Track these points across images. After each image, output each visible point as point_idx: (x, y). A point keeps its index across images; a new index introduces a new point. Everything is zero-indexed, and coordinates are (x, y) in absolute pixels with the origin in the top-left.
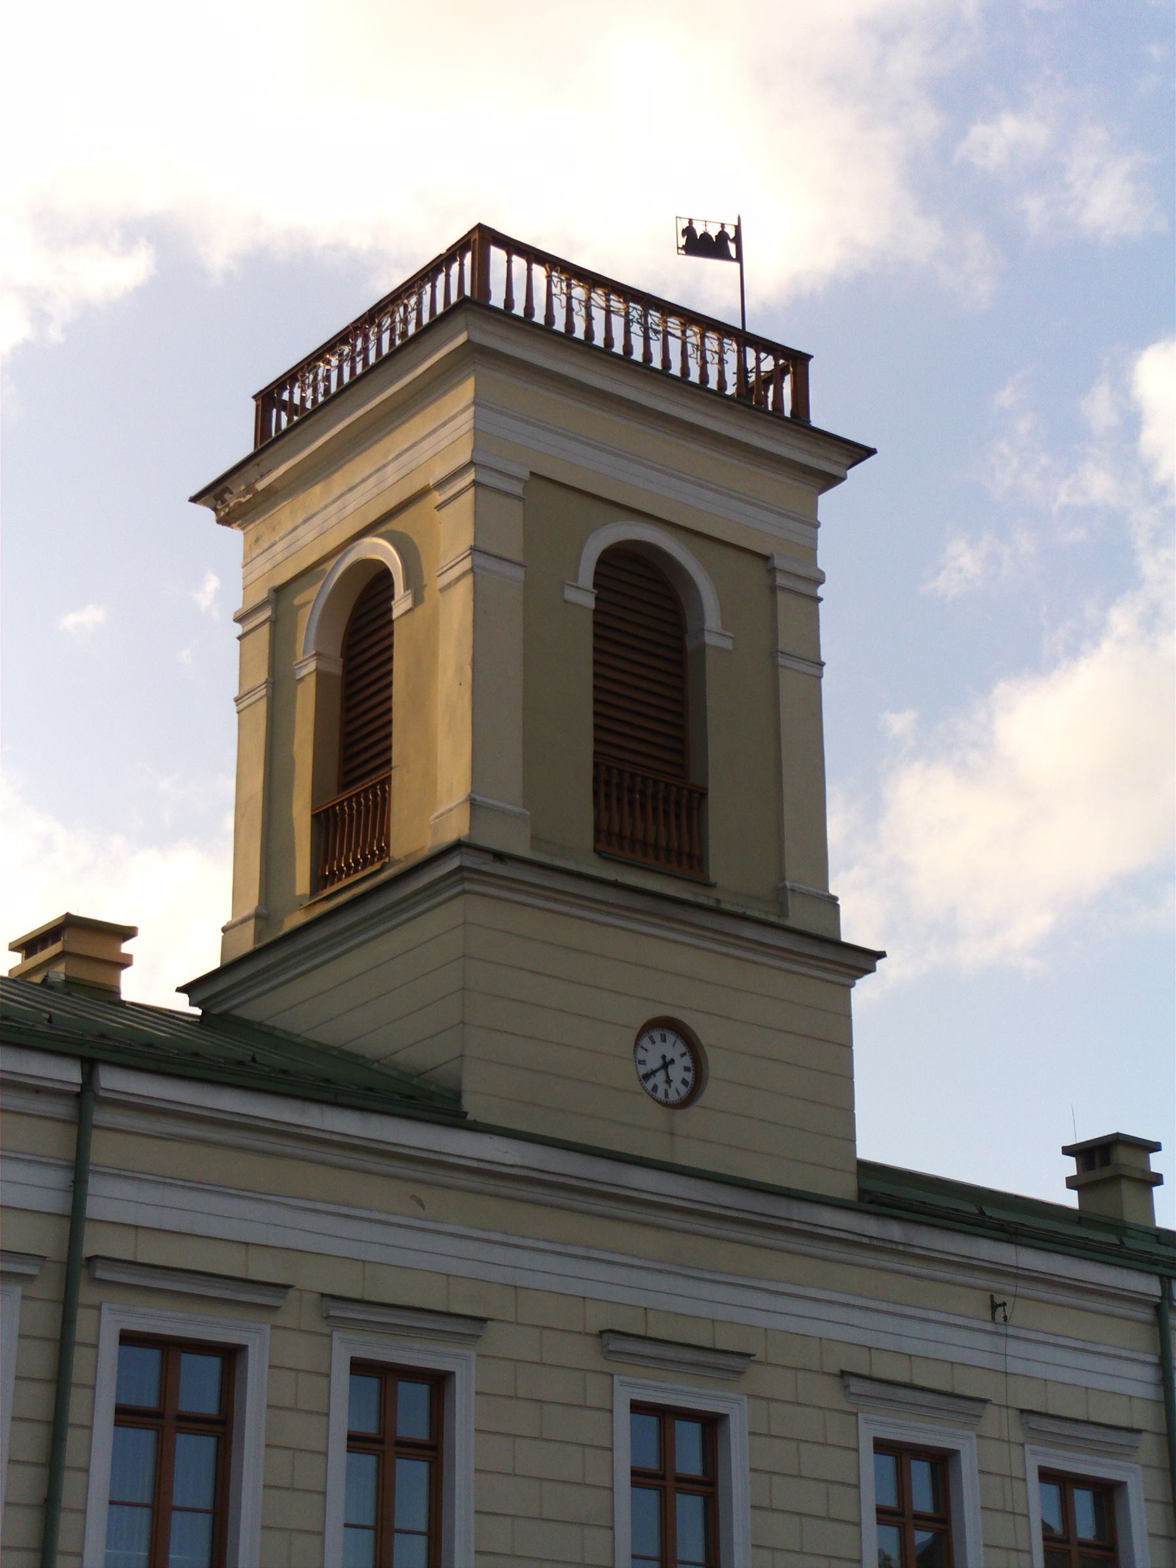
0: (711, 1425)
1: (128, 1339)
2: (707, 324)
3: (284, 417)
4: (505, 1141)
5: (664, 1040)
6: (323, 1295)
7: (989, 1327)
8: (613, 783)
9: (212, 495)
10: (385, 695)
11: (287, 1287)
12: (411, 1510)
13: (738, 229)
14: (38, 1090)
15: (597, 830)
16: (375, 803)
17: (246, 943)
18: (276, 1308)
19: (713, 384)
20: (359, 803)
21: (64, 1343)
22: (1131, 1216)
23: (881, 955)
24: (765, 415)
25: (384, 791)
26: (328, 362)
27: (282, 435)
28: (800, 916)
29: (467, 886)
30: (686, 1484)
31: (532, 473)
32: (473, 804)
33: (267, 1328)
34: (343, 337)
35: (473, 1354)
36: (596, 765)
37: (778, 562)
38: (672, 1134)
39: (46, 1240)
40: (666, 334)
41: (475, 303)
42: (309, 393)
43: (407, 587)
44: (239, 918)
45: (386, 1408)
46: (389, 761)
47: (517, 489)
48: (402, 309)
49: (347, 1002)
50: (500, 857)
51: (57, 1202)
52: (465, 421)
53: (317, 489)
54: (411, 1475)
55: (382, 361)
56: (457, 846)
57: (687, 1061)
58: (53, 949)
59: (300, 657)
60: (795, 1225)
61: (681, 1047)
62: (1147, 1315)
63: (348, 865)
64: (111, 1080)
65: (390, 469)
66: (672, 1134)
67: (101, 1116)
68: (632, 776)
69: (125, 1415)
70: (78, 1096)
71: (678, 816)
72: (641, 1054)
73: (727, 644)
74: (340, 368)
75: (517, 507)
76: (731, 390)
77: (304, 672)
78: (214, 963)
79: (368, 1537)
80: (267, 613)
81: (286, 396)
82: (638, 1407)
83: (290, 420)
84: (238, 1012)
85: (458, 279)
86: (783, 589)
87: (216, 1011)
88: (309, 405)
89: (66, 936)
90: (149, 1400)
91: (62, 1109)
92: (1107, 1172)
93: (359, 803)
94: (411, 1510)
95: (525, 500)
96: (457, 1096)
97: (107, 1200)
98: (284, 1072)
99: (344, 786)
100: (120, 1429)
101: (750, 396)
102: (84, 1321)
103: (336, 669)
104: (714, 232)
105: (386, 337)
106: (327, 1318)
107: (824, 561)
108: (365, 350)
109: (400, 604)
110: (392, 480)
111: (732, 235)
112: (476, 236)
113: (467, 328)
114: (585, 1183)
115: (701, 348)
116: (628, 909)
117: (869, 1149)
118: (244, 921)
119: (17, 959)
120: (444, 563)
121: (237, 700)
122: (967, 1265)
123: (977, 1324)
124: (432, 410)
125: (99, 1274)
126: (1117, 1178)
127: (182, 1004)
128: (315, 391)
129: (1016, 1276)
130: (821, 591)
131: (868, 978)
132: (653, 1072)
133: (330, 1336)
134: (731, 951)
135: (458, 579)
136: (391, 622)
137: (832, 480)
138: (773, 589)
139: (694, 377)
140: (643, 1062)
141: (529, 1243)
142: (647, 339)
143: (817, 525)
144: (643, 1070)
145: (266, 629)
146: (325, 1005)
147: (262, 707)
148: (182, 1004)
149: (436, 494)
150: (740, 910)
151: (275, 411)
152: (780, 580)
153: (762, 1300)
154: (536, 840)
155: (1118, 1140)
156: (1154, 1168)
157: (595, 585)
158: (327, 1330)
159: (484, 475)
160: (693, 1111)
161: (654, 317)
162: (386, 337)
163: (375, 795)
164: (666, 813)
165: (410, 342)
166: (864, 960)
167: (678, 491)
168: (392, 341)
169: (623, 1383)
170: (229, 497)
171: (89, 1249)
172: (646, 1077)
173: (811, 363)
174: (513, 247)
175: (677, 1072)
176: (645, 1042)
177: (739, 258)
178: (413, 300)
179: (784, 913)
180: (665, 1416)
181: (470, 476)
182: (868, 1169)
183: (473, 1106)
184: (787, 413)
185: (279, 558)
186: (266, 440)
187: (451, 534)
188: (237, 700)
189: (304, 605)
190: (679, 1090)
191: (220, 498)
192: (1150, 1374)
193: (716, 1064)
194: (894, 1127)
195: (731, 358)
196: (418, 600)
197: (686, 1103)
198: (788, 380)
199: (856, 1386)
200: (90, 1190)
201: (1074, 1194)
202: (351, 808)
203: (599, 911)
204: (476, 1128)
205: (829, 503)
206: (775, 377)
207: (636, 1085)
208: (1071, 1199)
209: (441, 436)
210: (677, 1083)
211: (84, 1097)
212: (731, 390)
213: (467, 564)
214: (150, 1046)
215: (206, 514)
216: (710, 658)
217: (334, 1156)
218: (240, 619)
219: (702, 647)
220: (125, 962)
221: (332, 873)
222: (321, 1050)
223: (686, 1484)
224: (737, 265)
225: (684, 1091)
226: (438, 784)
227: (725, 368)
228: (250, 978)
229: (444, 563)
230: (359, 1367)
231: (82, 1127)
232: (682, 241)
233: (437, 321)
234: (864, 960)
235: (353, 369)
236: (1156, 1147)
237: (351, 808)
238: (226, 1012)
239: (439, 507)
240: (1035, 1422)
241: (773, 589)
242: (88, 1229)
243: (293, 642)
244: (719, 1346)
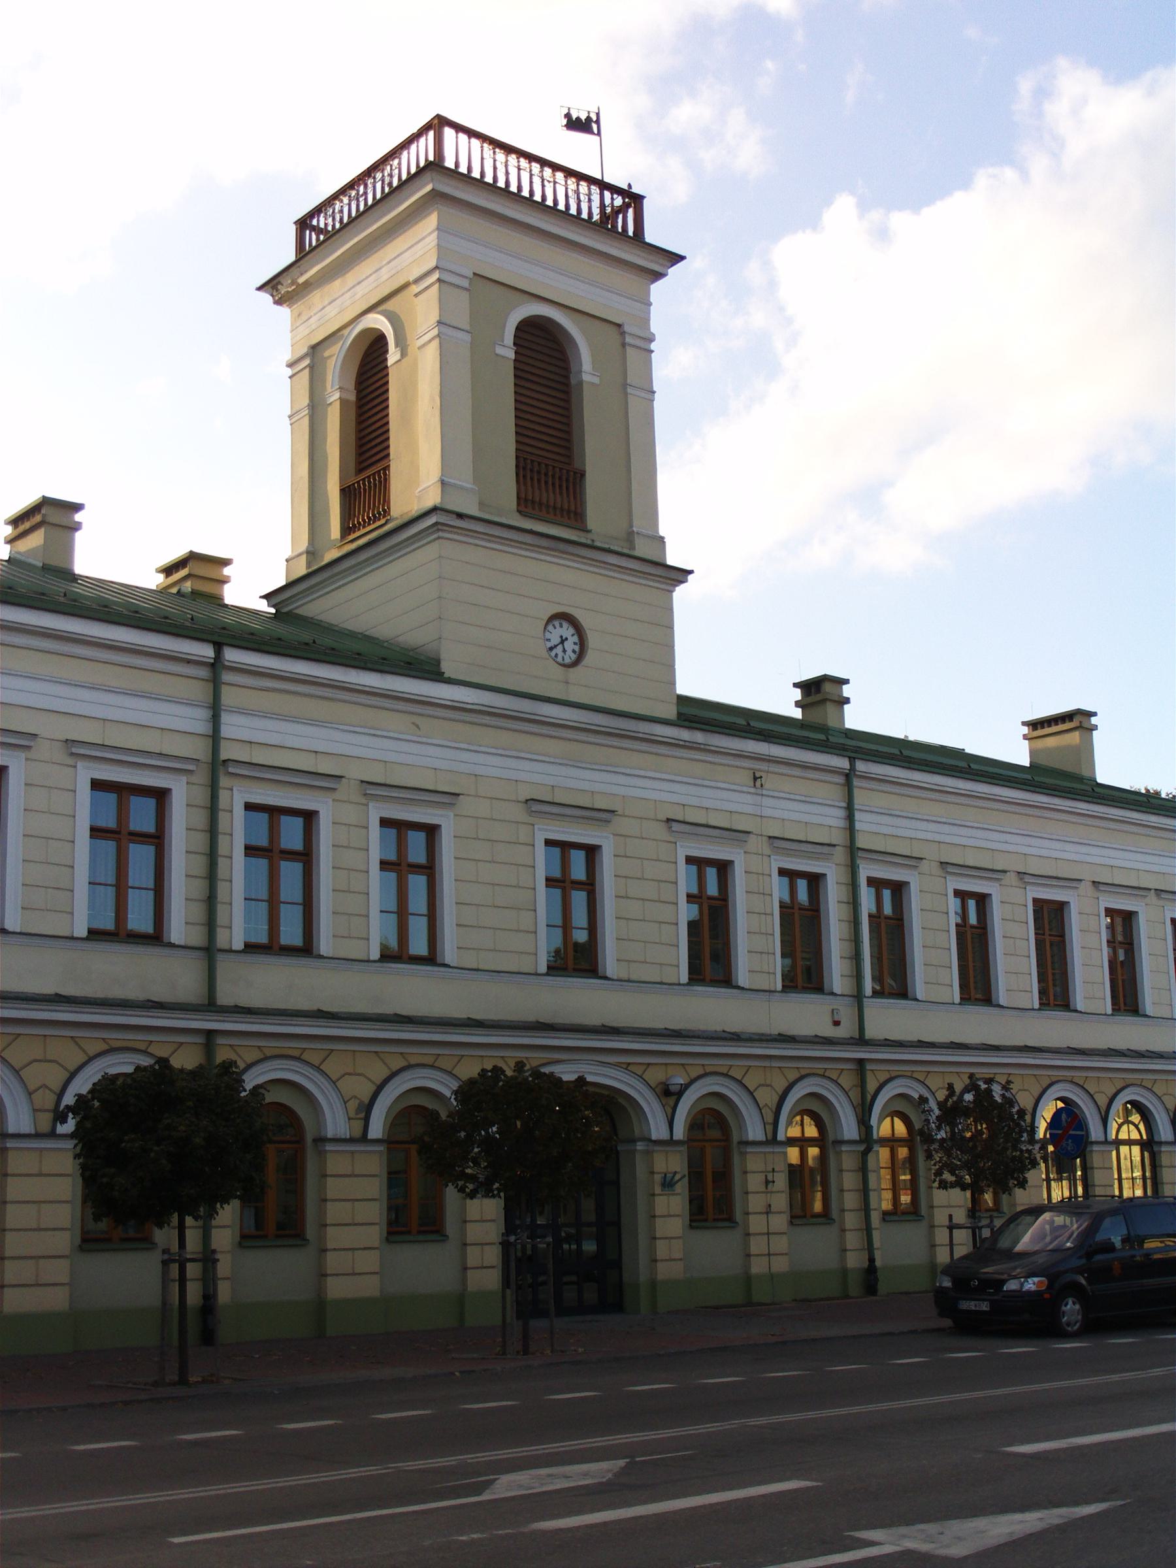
0: (592, 852)
1: (249, 807)
2: (580, 177)
3: (314, 236)
4: (503, 696)
5: (561, 626)
6: (362, 781)
7: (752, 790)
8: (526, 468)
9: (271, 285)
10: (384, 413)
11: (342, 777)
12: (418, 901)
13: (598, 114)
14: (189, 662)
15: (518, 498)
16: (380, 482)
17: (301, 570)
18: (28, 748)
19: (585, 215)
20: (369, 482)
21: (213, 809)
22: (832, 723)
23: (691, 572)
24: (617, 231)
25: (385, 474)
26: (342, 201)
27: (313, 249)
28: (642, 549)
29: (441, 534)
30: (577, 885)
31: (475, 274)
32: (443, 483)
33: (330, 801)
34: (351, 185)
35: (452, 814)
36: (517, 457)
37: (626, 328)
38: (567, 683)
39: (199, 750)
40: (555, 183)
41: (435, 166)
42: (330, 221)
43: (397, 346)
44: (296, 553)
45: (274, 831)
46: (388, 455)
47: (465, 283)
48: (389, 168)
49: (372, 603)
50: (460, 516)
51: (203, 727)
52: (432, 241)
53: (337, 283)
54: (141, 857)
55: (376, 203)
56: (434, 510)
57: (576, 639)
58: (183, 573)
59: (329, 389)
60: (641, 735)
61: (572, 630)
62: (841, 780)
63: (364, 520)
64: (232, 655)
65: (384, 270)
66: (567, 683)
67: (227, 677)
68: (539, 464)
69: (251, 850)
70: (213, 665)
71: (567, 488)
72: (548, 635)
73: (596, 380)
74: (349, 205)
75: (466, 295)
76: (596, 217)
77: (332, 399)
78: (284, 583)
79: (393, 918)
80: (307, 362)
81: (315, 222)
82: (549, 843)
83: (318, 239)
84: (296, 611)
85: (423, 150)
86: (630, 345)
87: (285, 610)
88: (330, 228)
89: (190, 564)
90: (263, 842)
91: (204, 673)
92: (818, 697)
93: (369, 482)
94: (418, 901)
95: (472, 289)
96: (438, 662)
97: (232, 725)
98: (333, 649)
99: (360, 471)
100: (253, 860)
101: (606, 223)
102: (223, 795)
103: (352, 397)
104: (583, 117)
105: (379, 186)
106: (72, 754)
107: (654, 328)
108: (365, 193)
109: (393, 356)
110: (385, 277)
111: (594, 118)
112: (436, 121)
113: (432, 180)
114: (516, 712)
115: (577, 192)
116: (539, 547)
117: (684, 687)
118: (300, 555)
119: (161, 578)
120: (420, 331)
121: (290, 417)
122: (740, 755)
123: (745, 789)
124: (410, 233)
125: (231, 770)
126: (824, 701)
127: (263, 606)
128: (334, 219)
129: (769, 761)
130: (653, 346)
131: (683, 586)
132: (556, 646)
133: (367, 805)
134: (602, 571)
135: (430, 341)
136: (387, 367)
137: (658, 276)
138: (624, 345)
139: (573, 211)
140: (549, 640)
141: (483, 749)
142: (543, 186)
143: (650, 304)
144: (549, 645)
145: (307, 371)
146: (352, 606)
147: (306, 420)
148: (263, 606)
149: (414, 287)
150: (606, 546)
151: (308, 232)
152: (628, 339)
153: (621, 779)
154: (482, 505)
155: (825, 679)
156: (845, 695)
157: (515, 344)
158: (364, 801)
159: (445, 275)
160: (579, 668)
161: (548, 172)
162: (379, 186)
163: (380, 477)
164: (560, 486)
165: (393, 191)
166: (681, 575)
167: (564, 284)
168: (383, 188)
169: (540, 829)
170: (279, 287)
171: (224, 755)
172: (551, 649)
173: (645, 201)
174: (459, 128)
175: (569, 645)
176: (550, 627)
177: (599, 134)
178: (396, 162)
179: (633, 548)
180: (565, 847)
181: (436, 276)
182: (683, 700)
183: (448, 668)
184: (631, 233)
185: (313, 327)
186: (303, 253)
187: (424, 313)
188: (290, 417)
189: (329, 357)
190: (570, 657)
191: (275, 288)
192: (842, 813)
193: (592, 640)
194: (697, 678)
195: (596, 198)
196: (404, 354)
197: (575, 663)
198: (631, 212)
199: (676, 827)
200: (223, 721)
201: (800, 710)
202: (364, 485)
203: (521, 548)
204: (450, 681)
205: (657, 289)
206: (623, 209)
207: (545, 654)
208: (797, 714)
209: (417, 249)
210: (569, 652)
211: (216, 665)
212: (596, 217)
213: (435, 332)
214: (252, 634)
215: (266, 298)
216: (585, 386)
217: (362, 699)
218: (290, 365)
219: (580, 383)
220: (224, 581)
221: (354, 525)
222: (352, 635)
223: (577, 885)
224: (597, 138)
225: (574, 657)
226: (420, 470)
227: (591, 203)
228: (305, 590)
229: (420, 331)
230: (385, 823)
231: (216, 683)
232: (565, 122)
233: (411, 178)
234: (681, 575)
235: (358, 206)
236: (846, 682)
237: (364, 485)
238: (290, 611)
239: (416, 295)
240: (537, 807)
241: (624, 345)
242: (223, 744)
243: (324, 381)
244: (596, 806)
